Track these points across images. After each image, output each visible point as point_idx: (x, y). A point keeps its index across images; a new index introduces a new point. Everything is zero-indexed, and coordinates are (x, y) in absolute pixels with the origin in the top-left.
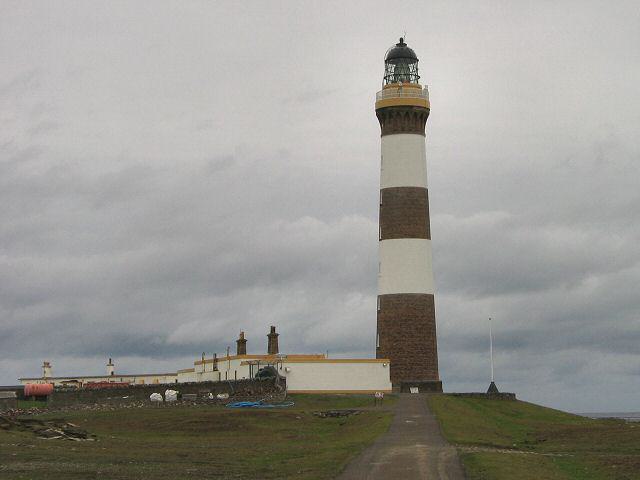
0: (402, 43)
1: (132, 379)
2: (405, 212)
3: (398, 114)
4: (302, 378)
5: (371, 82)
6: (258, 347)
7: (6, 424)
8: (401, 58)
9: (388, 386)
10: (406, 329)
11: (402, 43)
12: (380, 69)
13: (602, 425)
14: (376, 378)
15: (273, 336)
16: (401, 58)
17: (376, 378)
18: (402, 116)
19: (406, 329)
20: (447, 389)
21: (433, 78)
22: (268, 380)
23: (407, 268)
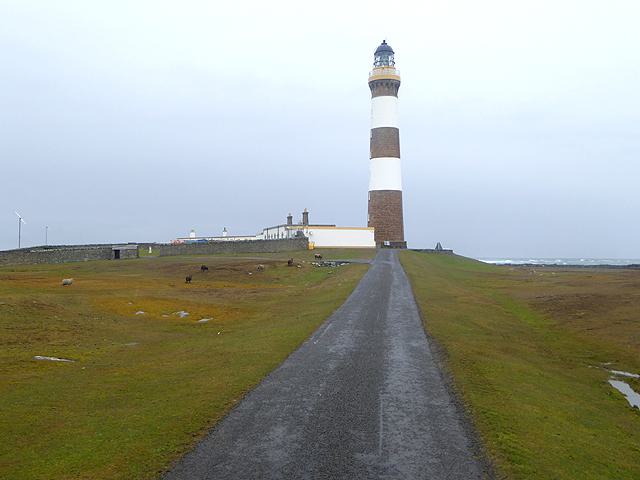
0: (384, 43)
1: (275, 231)
2: (385, 143)
3: (387, 84)
4: (319, 238)
5: (365, 68)
6: (298, 219)
7: (4, 279)
8: (384, 52)
9: (373, 244)
10: (386, 210)
11: (384, 43)
12: (372, 59)
13: (491, 328)
14: (366, 239)
15: (306, 214)
16: (384, 52)
17: (366, 239)
18: (385, 86)
19: (386, 210)
20: (409, 247)
21: (402, 67)
22: (301, 240)
23: (386, 175)
